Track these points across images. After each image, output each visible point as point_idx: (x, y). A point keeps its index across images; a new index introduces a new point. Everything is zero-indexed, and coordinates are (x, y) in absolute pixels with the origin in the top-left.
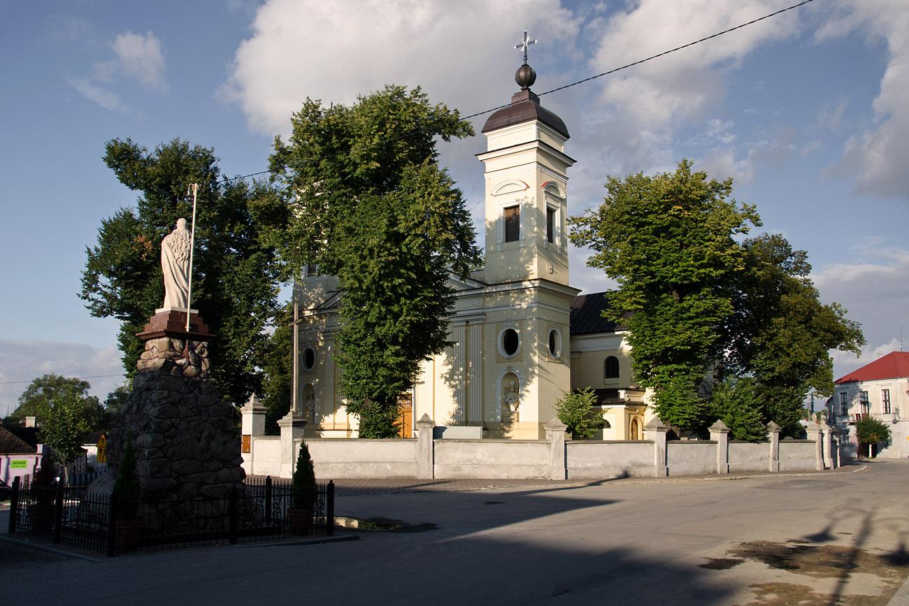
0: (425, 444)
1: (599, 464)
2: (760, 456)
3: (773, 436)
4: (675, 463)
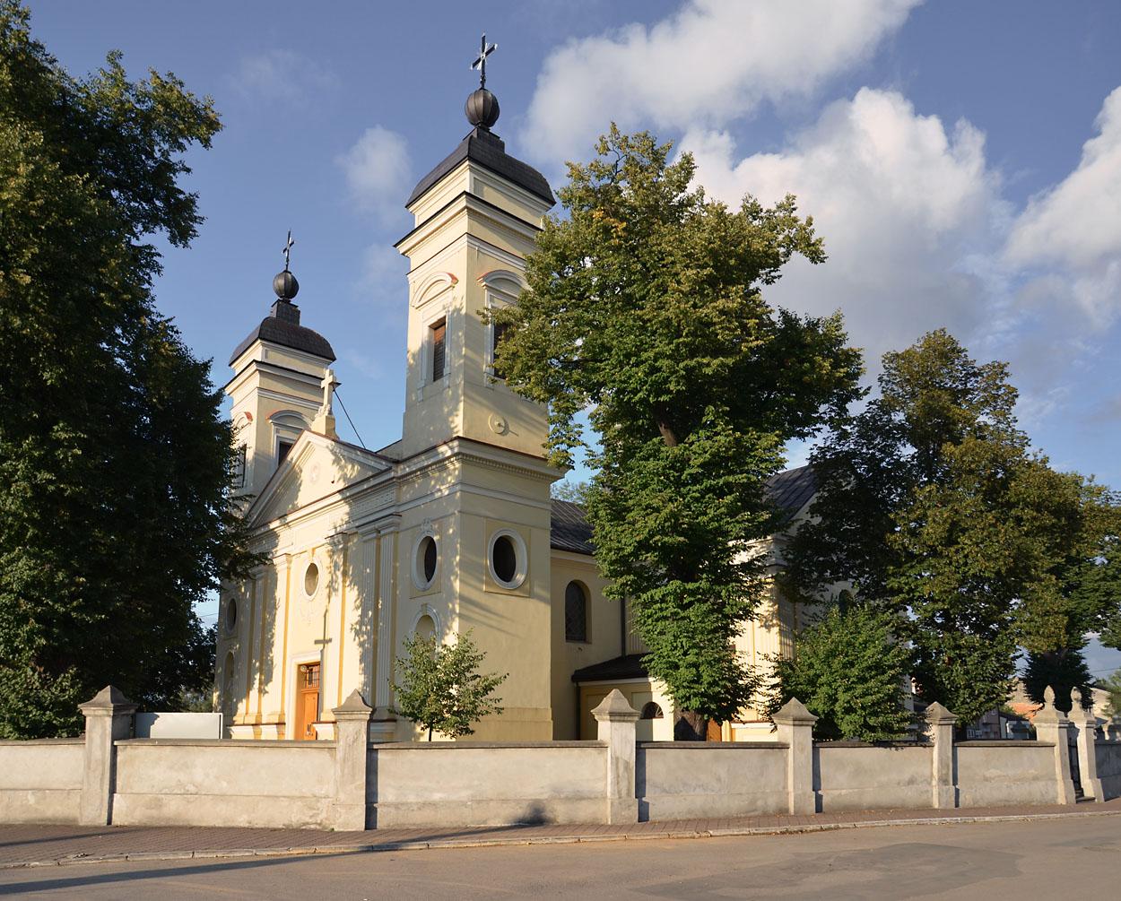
0: (97, 754)
1: (464, 795)
2: (906, 777)
3: (937, 736)
4: (664, 791)
